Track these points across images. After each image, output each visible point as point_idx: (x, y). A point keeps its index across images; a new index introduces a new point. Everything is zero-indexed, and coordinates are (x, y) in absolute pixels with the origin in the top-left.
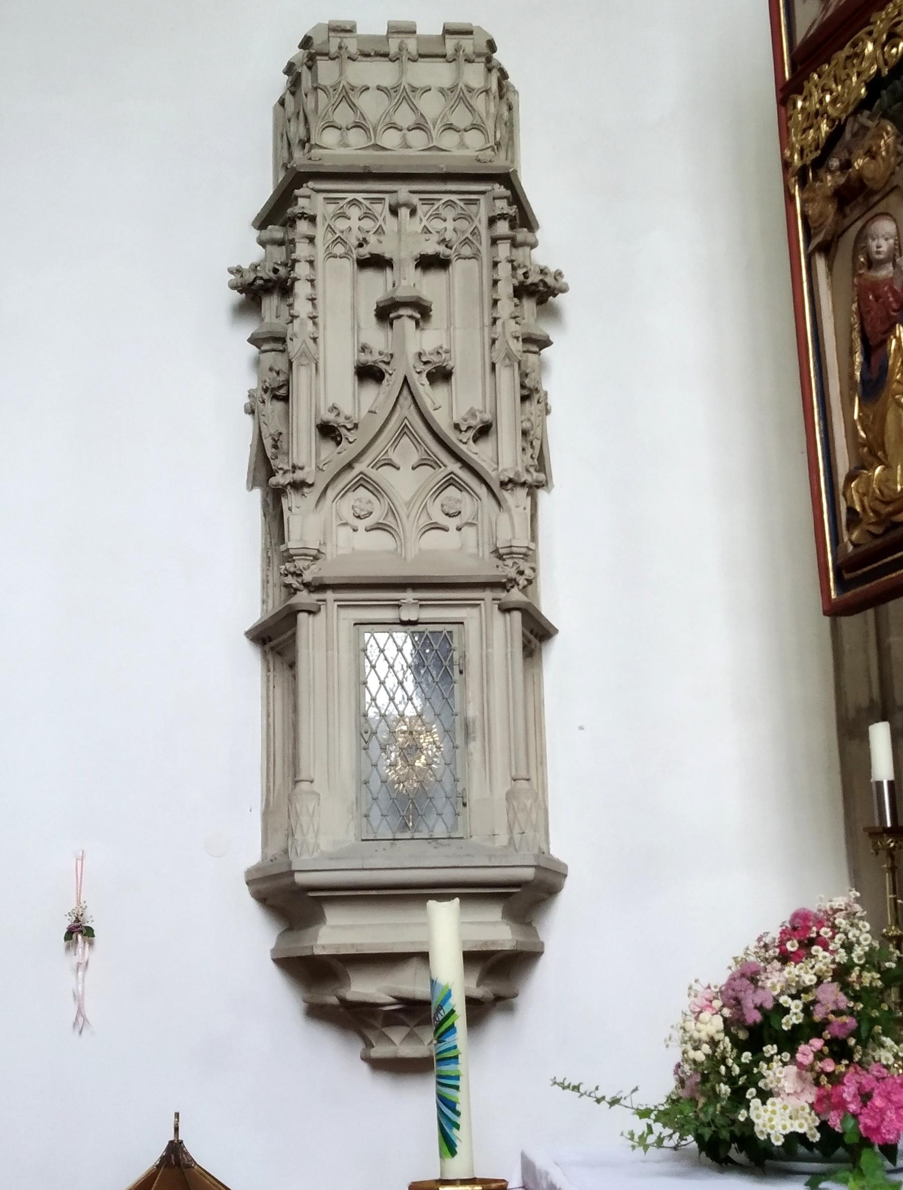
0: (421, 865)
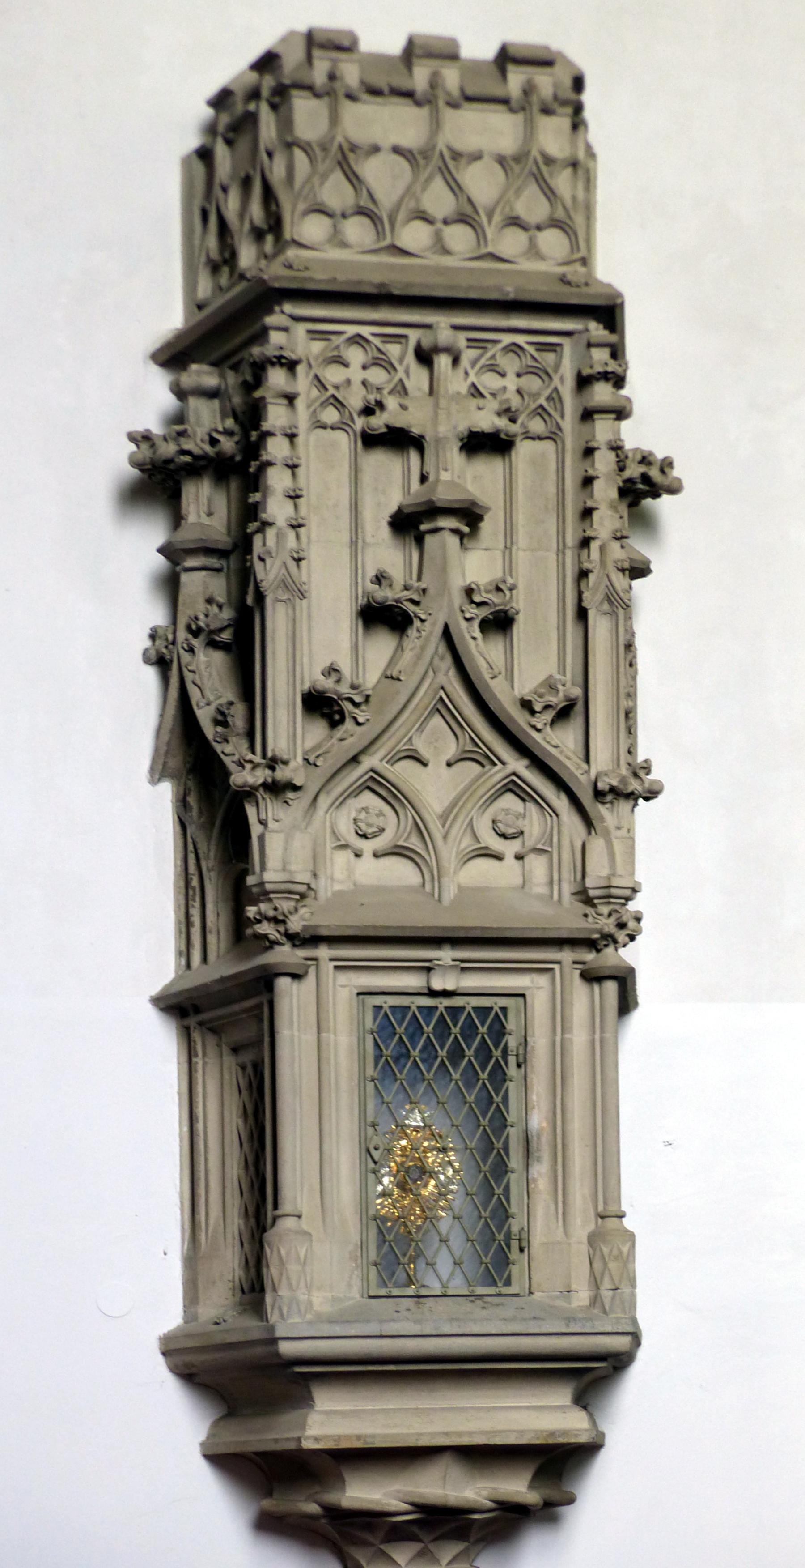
0: (467, 1331)
